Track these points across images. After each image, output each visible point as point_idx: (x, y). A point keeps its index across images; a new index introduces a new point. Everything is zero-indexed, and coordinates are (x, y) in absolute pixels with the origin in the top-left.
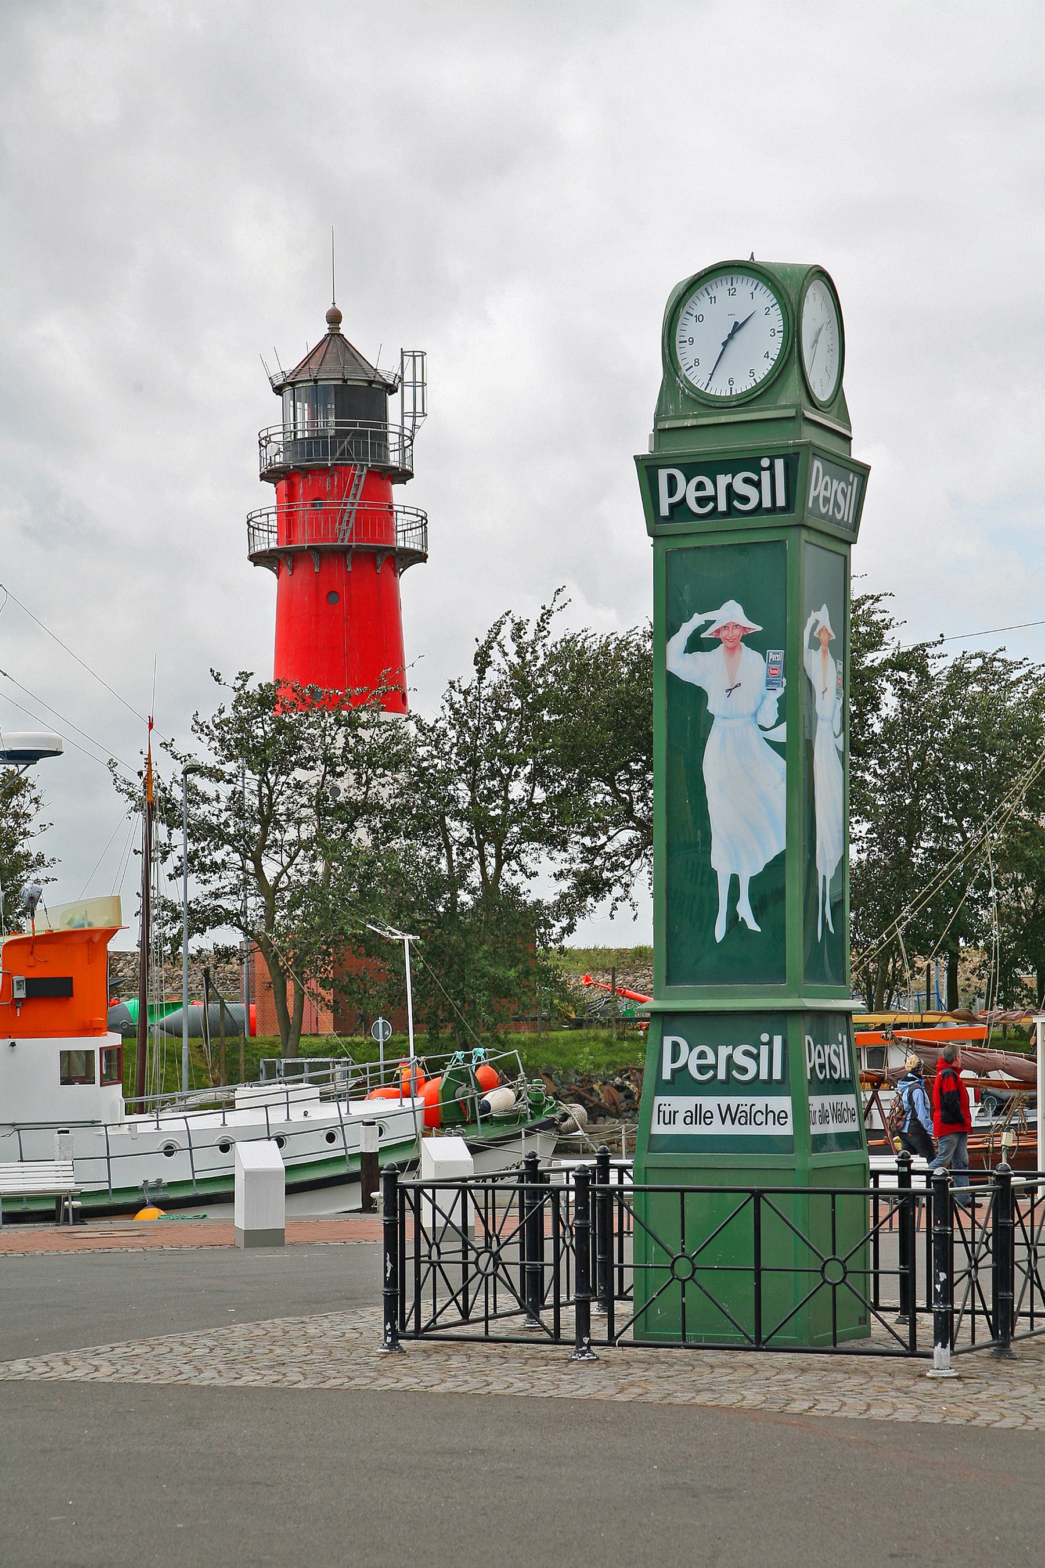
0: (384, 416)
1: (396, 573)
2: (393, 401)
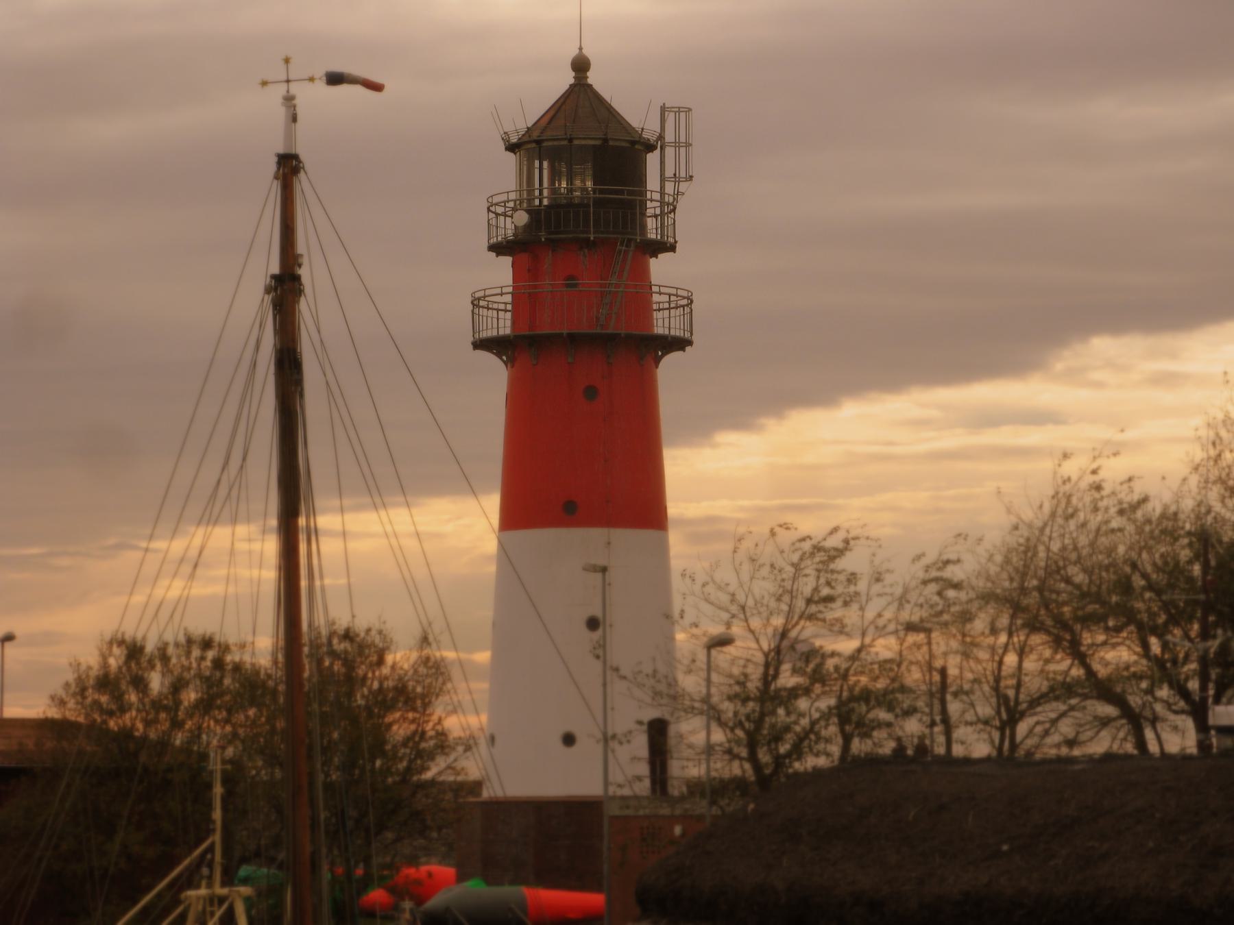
0: (640, 180)
1: (657, 361)
2: (652, 159)
